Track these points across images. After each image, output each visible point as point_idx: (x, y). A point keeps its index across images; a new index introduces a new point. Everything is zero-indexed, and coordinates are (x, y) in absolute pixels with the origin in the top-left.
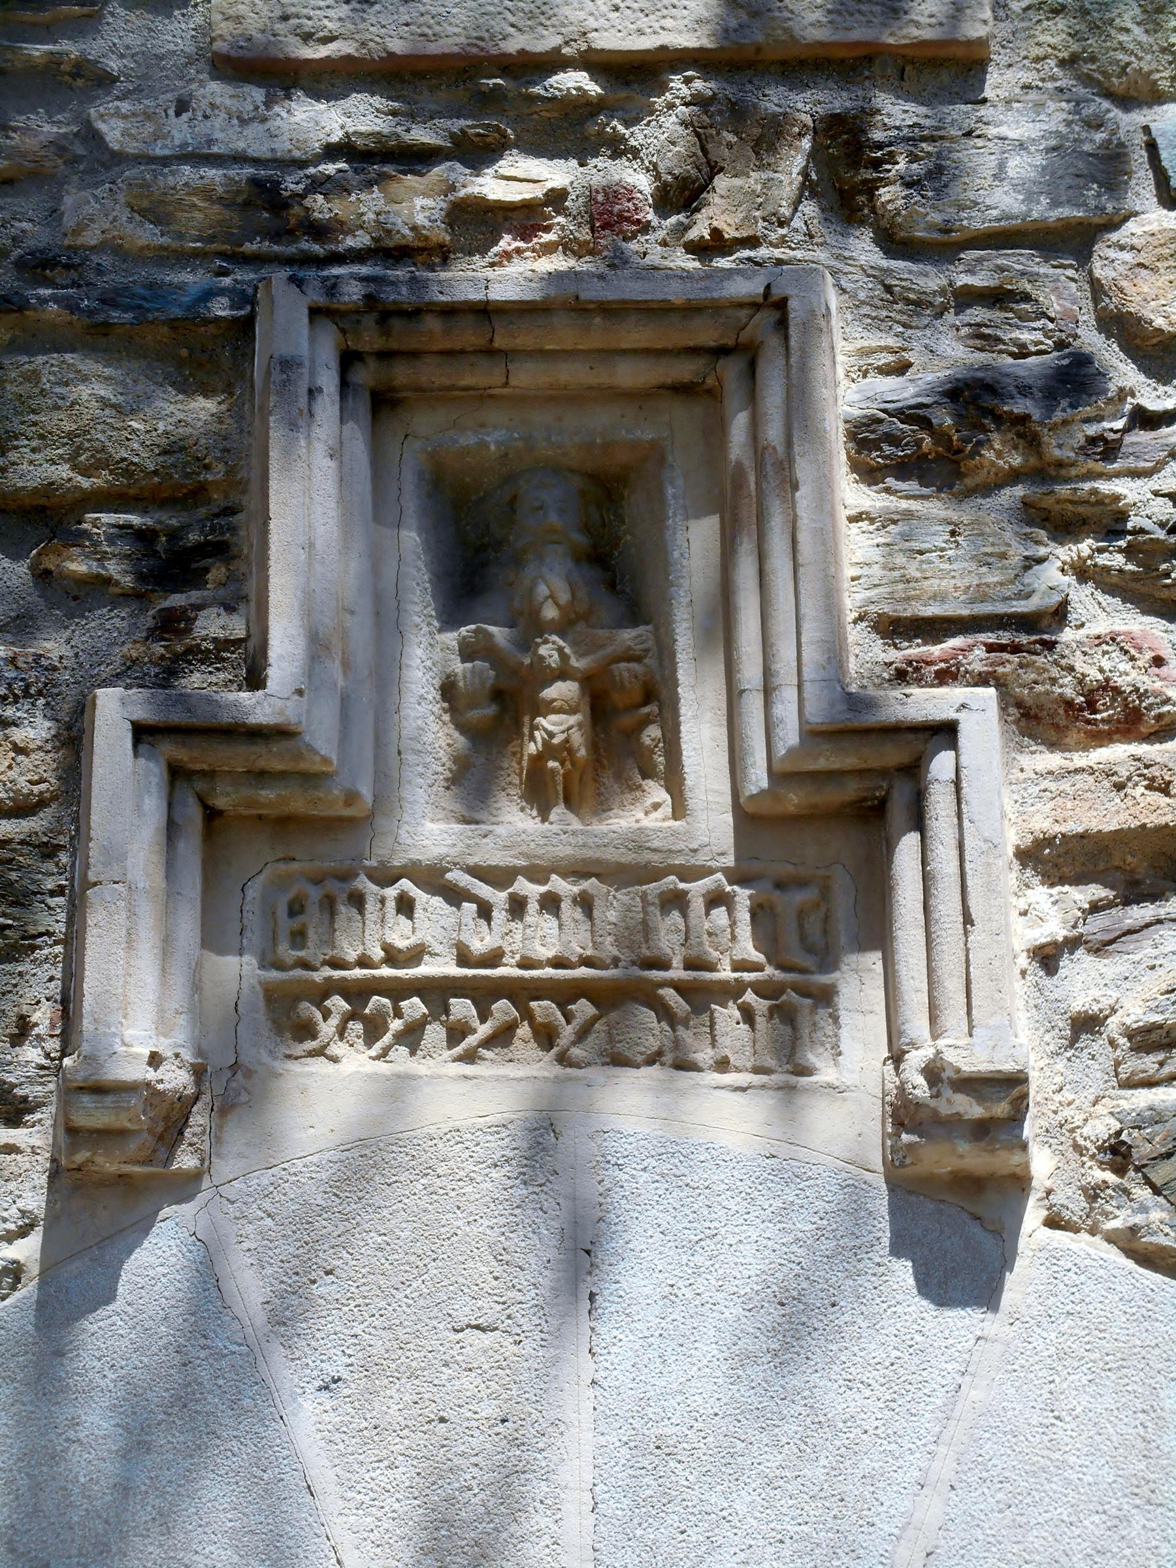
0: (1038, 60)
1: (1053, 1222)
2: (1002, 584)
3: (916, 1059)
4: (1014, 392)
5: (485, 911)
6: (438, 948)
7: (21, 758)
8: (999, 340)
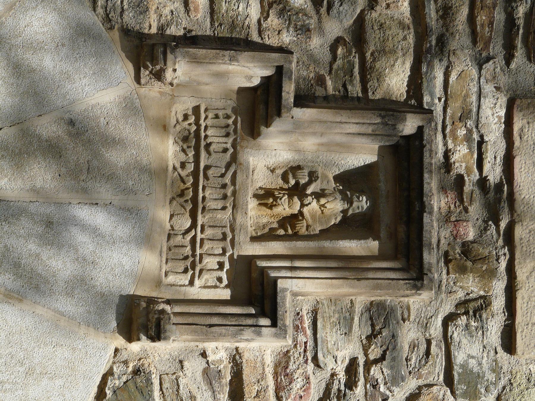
0: (511, 372)
1: (116, 350)
2: (327, 348)
3: (168, 308)
4: (393, 356)
5: (223, 176)
6: (210, 160)
7: (277, 32)
8: (412, 352)
